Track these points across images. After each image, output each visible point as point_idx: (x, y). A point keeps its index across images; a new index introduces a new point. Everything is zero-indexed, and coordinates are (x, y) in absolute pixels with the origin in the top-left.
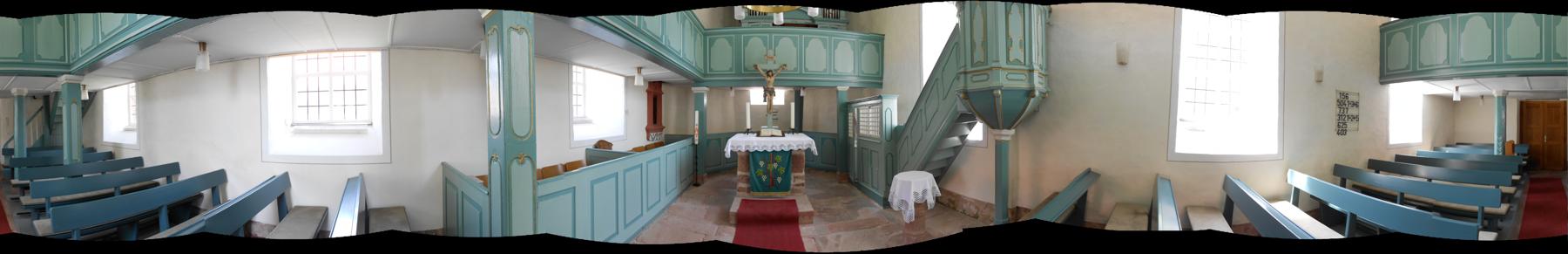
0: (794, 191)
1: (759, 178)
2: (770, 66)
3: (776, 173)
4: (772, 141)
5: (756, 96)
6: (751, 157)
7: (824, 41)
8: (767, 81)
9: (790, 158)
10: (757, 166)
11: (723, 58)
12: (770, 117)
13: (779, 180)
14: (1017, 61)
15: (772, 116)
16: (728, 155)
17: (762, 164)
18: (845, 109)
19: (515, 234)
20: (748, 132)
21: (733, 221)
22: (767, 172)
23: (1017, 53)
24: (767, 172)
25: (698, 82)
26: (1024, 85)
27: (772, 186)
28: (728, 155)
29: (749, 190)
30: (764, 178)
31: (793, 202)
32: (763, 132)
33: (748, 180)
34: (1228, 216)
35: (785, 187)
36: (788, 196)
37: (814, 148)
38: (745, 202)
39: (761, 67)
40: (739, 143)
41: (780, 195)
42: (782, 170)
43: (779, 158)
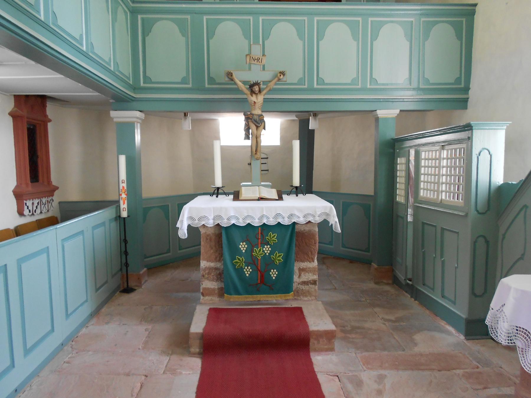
0: (298, 294)
1: (240, 272)
2: (255, 75)
3: (269, 263)
4: (260, 208)
5: (230, 129)
6: (224, 236)
7: (353, 27)
9: (293, 237)
10: (235, 251)
11: (168, 57)
12: (257, 166)
13: (274, 274)
16: (183, 233)
17: (243, 247)
18: (390, 150)
20: (217, 192)
21: (195, 349)
22: (252, 262)
24: (252, 262)
25: (122, 101)
27: (261, 284)
28: (183, 233)
29: (221, 293)
30: (248, 271)
32: (245, 193)
33: (220, 275)
35: (284, 286)
37: (334, 220)
38: (215, 314)
40: (202, 212)
42: (279, 258)
43: (273, 237)
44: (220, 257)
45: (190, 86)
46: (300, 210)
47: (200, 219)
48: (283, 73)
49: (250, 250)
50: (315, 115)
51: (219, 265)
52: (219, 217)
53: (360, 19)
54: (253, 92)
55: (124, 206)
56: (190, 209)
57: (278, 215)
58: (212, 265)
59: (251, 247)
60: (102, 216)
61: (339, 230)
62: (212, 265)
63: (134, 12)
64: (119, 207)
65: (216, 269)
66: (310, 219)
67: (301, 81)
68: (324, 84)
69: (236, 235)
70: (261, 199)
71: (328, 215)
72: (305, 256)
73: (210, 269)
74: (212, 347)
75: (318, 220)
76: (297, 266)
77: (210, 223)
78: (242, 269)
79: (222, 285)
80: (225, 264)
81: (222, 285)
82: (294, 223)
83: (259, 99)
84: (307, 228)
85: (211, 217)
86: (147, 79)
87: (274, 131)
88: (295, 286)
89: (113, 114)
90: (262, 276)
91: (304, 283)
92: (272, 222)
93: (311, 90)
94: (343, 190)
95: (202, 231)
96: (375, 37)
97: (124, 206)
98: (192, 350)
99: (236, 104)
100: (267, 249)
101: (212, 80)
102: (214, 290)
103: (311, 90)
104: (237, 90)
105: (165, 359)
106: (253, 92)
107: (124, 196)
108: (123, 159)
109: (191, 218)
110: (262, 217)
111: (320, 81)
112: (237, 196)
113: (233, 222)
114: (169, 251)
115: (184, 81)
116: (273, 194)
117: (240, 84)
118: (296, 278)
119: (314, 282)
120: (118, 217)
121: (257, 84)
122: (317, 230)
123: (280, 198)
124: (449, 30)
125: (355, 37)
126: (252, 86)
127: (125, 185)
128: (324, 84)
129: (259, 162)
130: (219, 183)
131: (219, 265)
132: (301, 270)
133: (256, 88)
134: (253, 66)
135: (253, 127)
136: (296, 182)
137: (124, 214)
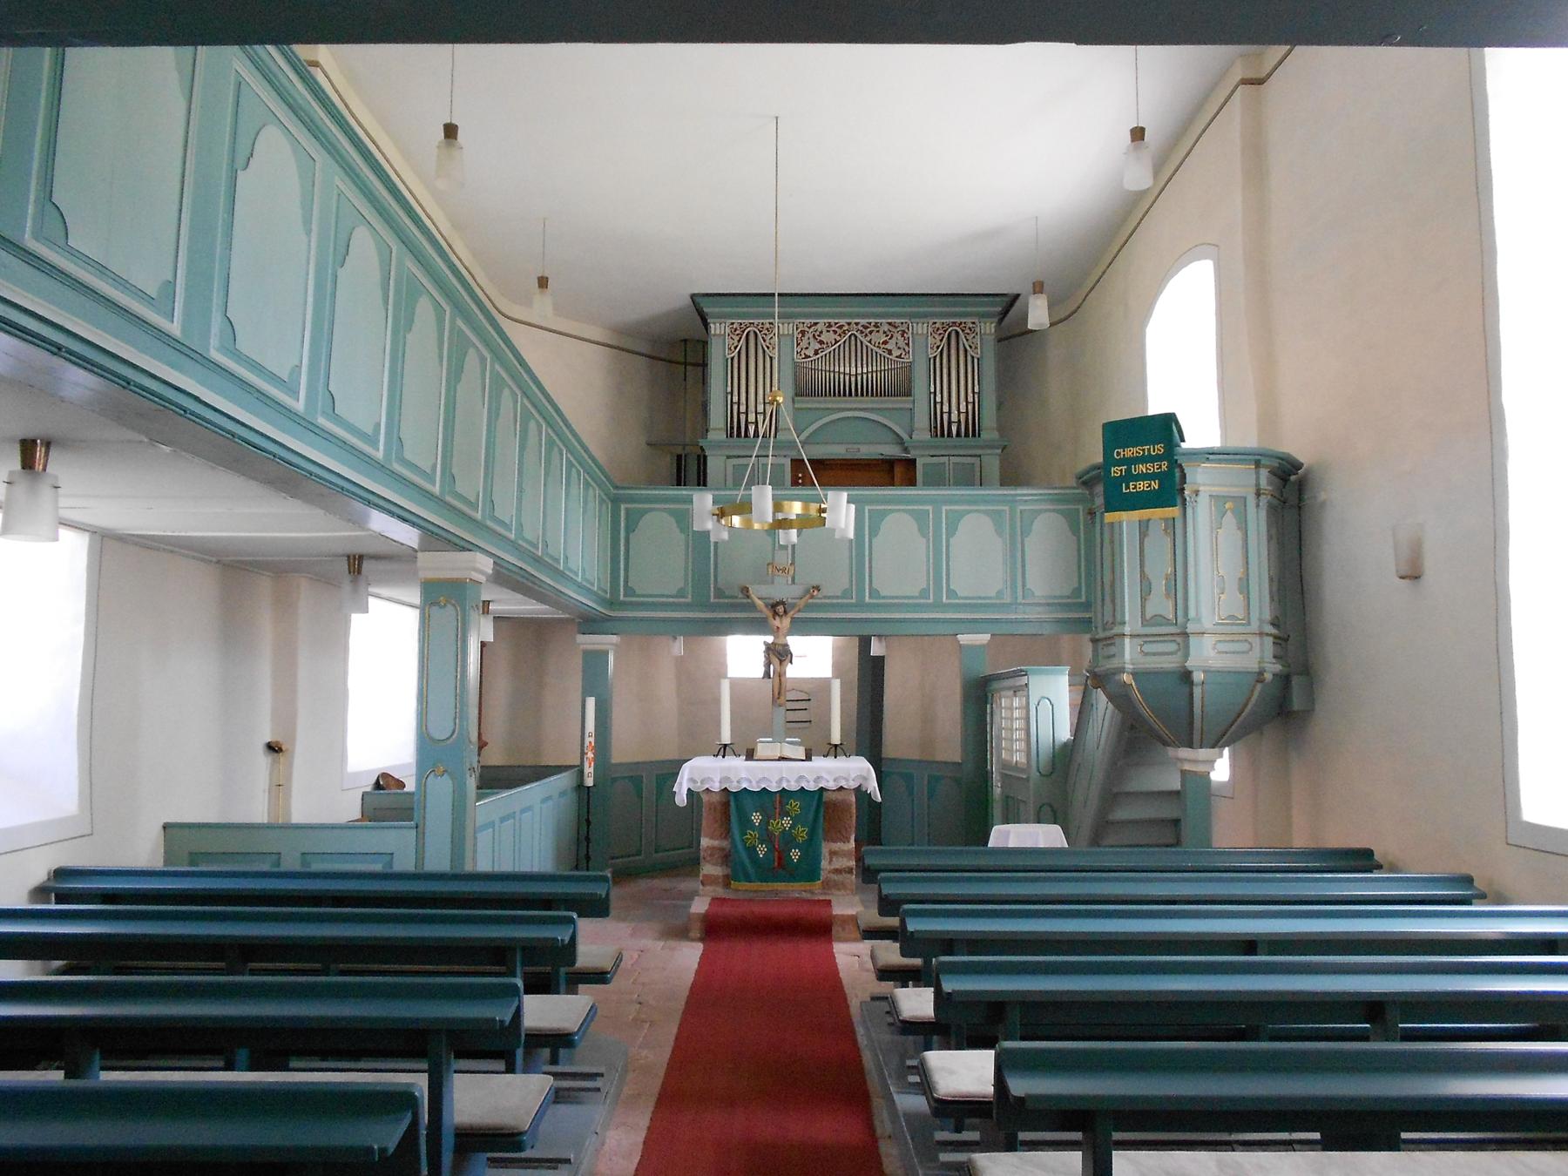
0: (827, 885)
1: (752, 851)
2: (782, 589)
3: (789, 839)
4: (782, 768)
5: (743, 655)
6: (733, 803)
7: (920, 518)
8: (776, 617)
9: (820, 807)
10: (746, 823)
11: (660, 568)
12: (780, 716)
13: (795, 855)
14: (1159, 620)
15: (791, 709)
16: (681, 799)
17: (756, 818)
18: (979, 695)
19: (1150, 413)
20: (724, 750)
21: (696, 933)
22: (767, 837)
23: (1160, 604)
24: (767, 837)
25: (590, 623)
26: (1169, 663)
27: (779, 868)
28: (681, 799)
29: (726, 881)
30: (762, 850)
31: (829, 902)
32: (761, 750)
33: (726, 857)
34: (868, 735)
35: (809, 871)
36: (815, 891)
37: (872, 786)
38: (716, 901)
39: (759, 593)
40: (703, 773)
41: (796, 890)
42: (802, 833)
43: (794, 805)
44: (727, 833)
45: (689, 600)
46: (829, 772)
47: (702, 782)
48: (818, 588)
49: (765, 822)
50: (879, 636)
51: (725, 844)
52: (727, 779)
53: (930, 508)
54: (776, 614)
55: (589, 770)
56: (692, 769)
57: (801, 777)
58: (716, 843)
59: (767, 818)
60: (562, 781)
61: (879, 799)
62: (716, 843)
63: (616, 501)
64: (581, 772)
65: (722, 849)
66: (843, 784)
67: (846, 594)
68: (879, 597)
69: (748, 803)
70: (782, 759)
71: (865, 779)
72: (837, 834)
73: (713, 848)
74: (714, 929)
75: (853, 785)
76: (825, 848)
77: (716, 787)
78: (754, 848)
79: (728, 871)
80: (733, 843)
81: (728, 871)
82: (822, 789)
83: (786, 621)
84: (840, 796)
85: (717, 779)
86: (629, 591)
87: (815, 657)
88: (823, 875)
89: (581, 638)
90: (780, 858)
91: (837, 871)
92: (794, 787)
93: (861, 605)
94: (940, 757)
95: (705, 797)
96: (952, 531)
97: (589, 770)
98: (692, 934)
99: (756, 625)
100: (787, 822)
101: (720, 593)
102: (717, 878)
103: (861, 605)
104: (753, 607)
105: (662, 943)
106: (776, 614)
107: (590, 755)
108: (591, 703)
109: (692, 780)
110: (781, 780)
111: (874, 593)
112: (750, 755)
113: (744, 785)
114: (639, 853)
115: (681, 593)
116: (800, 752)
117: (759, 603)
118: (824, 864)
119: (850, 871)
120: (580, 786)
121: (782, 603)
122: (854, 799)
123: (808, 758)
124: (1059, 521)
125: (923, 531)
126: (774, 606)
127: (592, 740)
128: (879, 597)
129: (782, 710)
130: (726, 737)
131: (725, 844)
132: (833, 853)
133: (780, 609)
134: (777, 579)
135: (776, 661)
136: (836, 738)
137: (589, 782)
